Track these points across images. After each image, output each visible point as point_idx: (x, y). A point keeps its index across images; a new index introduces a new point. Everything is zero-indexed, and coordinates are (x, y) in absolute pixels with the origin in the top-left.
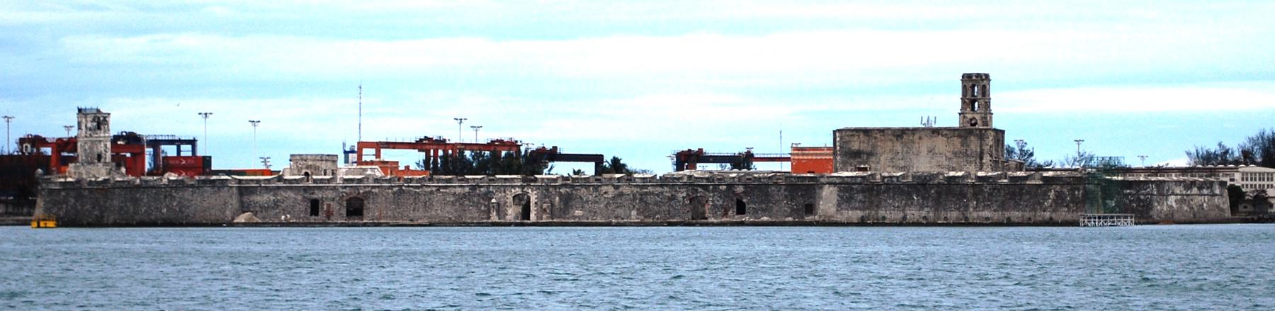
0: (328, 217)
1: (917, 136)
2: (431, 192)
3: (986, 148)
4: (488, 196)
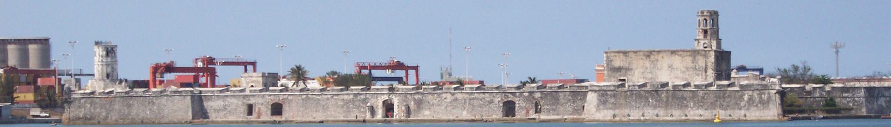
0: (259, 117)
1: (661, 55)
2: (328, 99)
3: (709, 64)
4: (365, 101)
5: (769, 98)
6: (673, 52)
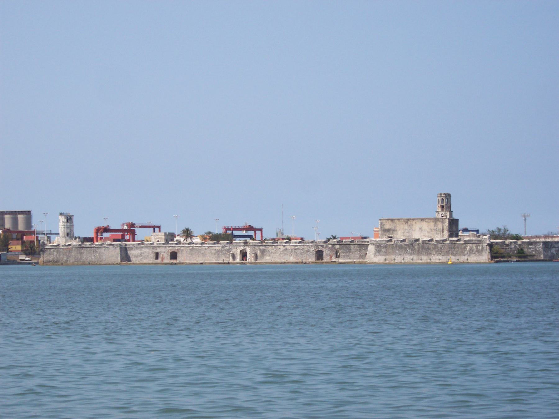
5: (483, 248)
6: (422, 220)
